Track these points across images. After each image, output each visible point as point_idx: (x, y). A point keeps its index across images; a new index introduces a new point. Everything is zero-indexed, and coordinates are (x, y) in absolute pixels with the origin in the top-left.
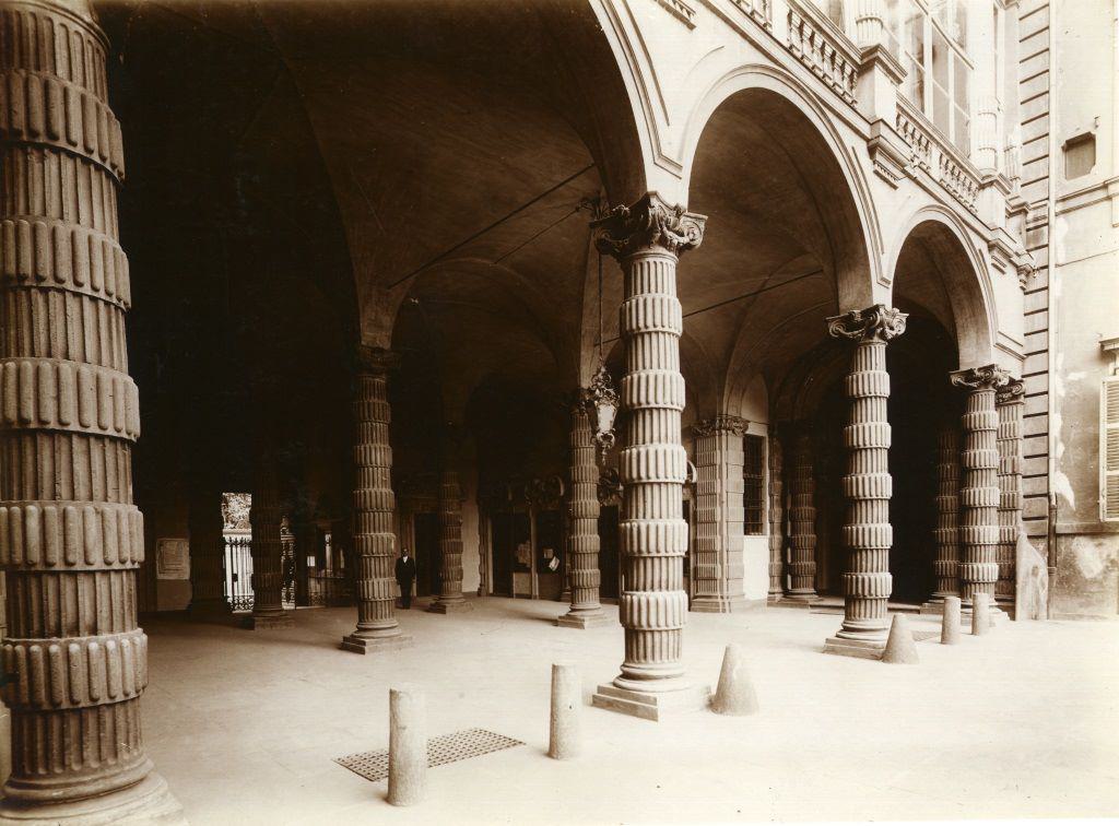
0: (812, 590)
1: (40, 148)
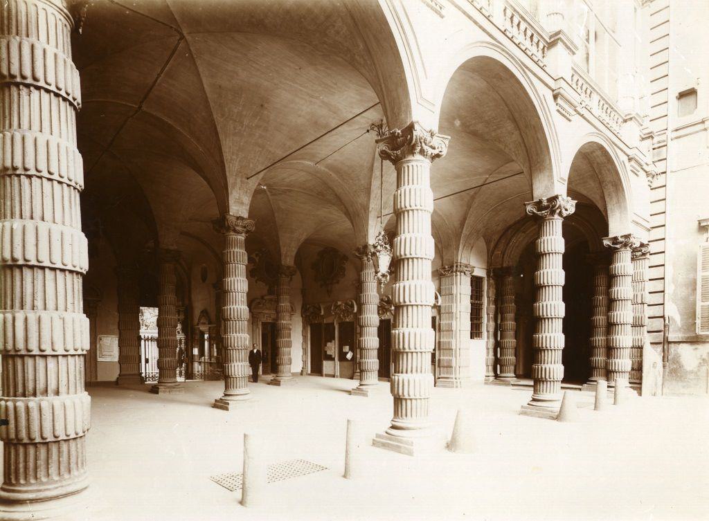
0: (514, 375)
1: (28, 86)
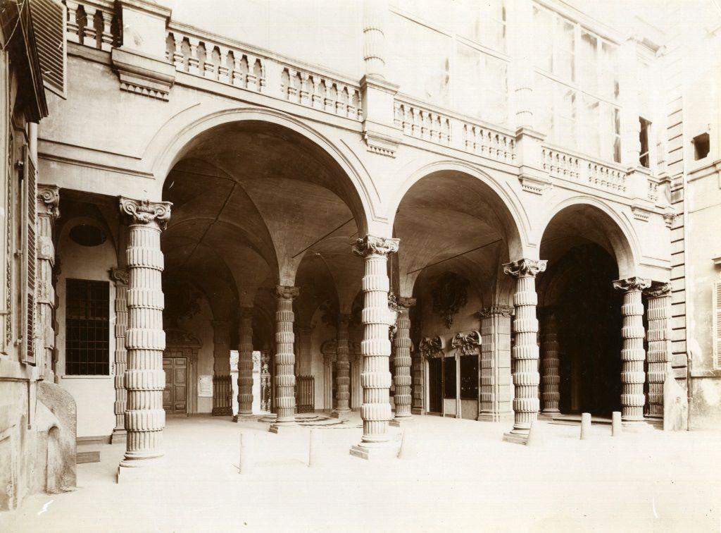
0: (557, 410)
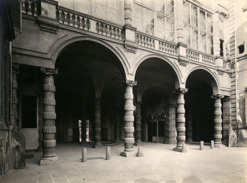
1: (48, 91)
